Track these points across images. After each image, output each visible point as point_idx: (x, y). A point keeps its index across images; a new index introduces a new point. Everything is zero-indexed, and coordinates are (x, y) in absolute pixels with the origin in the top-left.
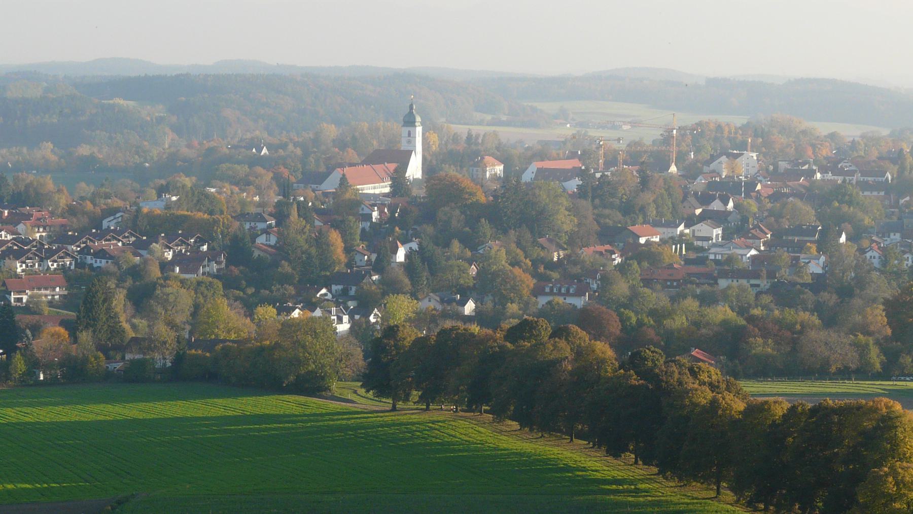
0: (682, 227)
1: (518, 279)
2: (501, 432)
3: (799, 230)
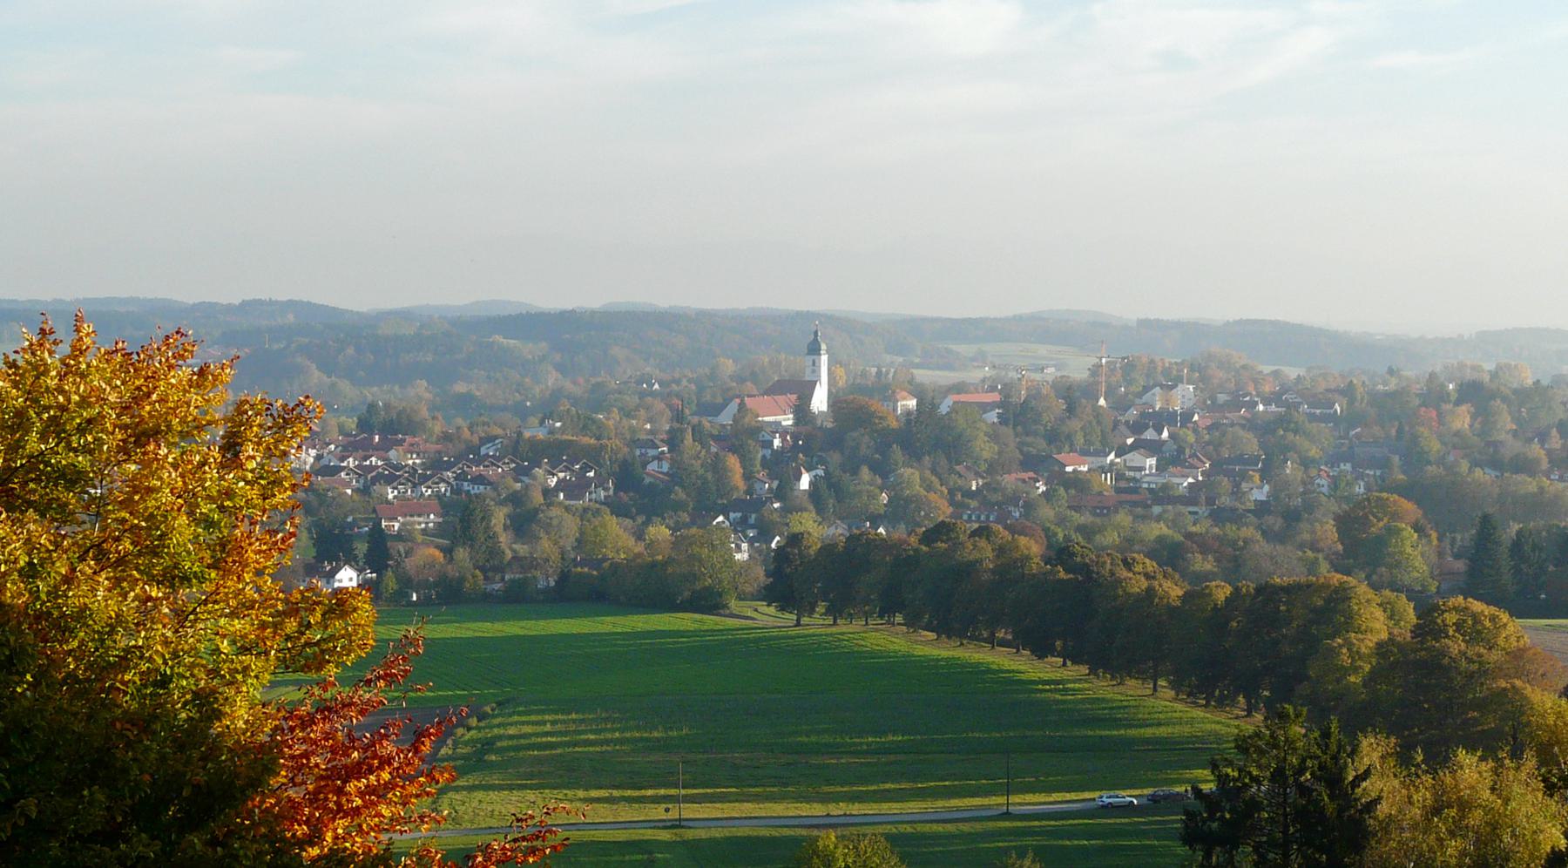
0: (1112, 456)
1: (933, 505)
2: (916, 642)
3: (1240, 459)
